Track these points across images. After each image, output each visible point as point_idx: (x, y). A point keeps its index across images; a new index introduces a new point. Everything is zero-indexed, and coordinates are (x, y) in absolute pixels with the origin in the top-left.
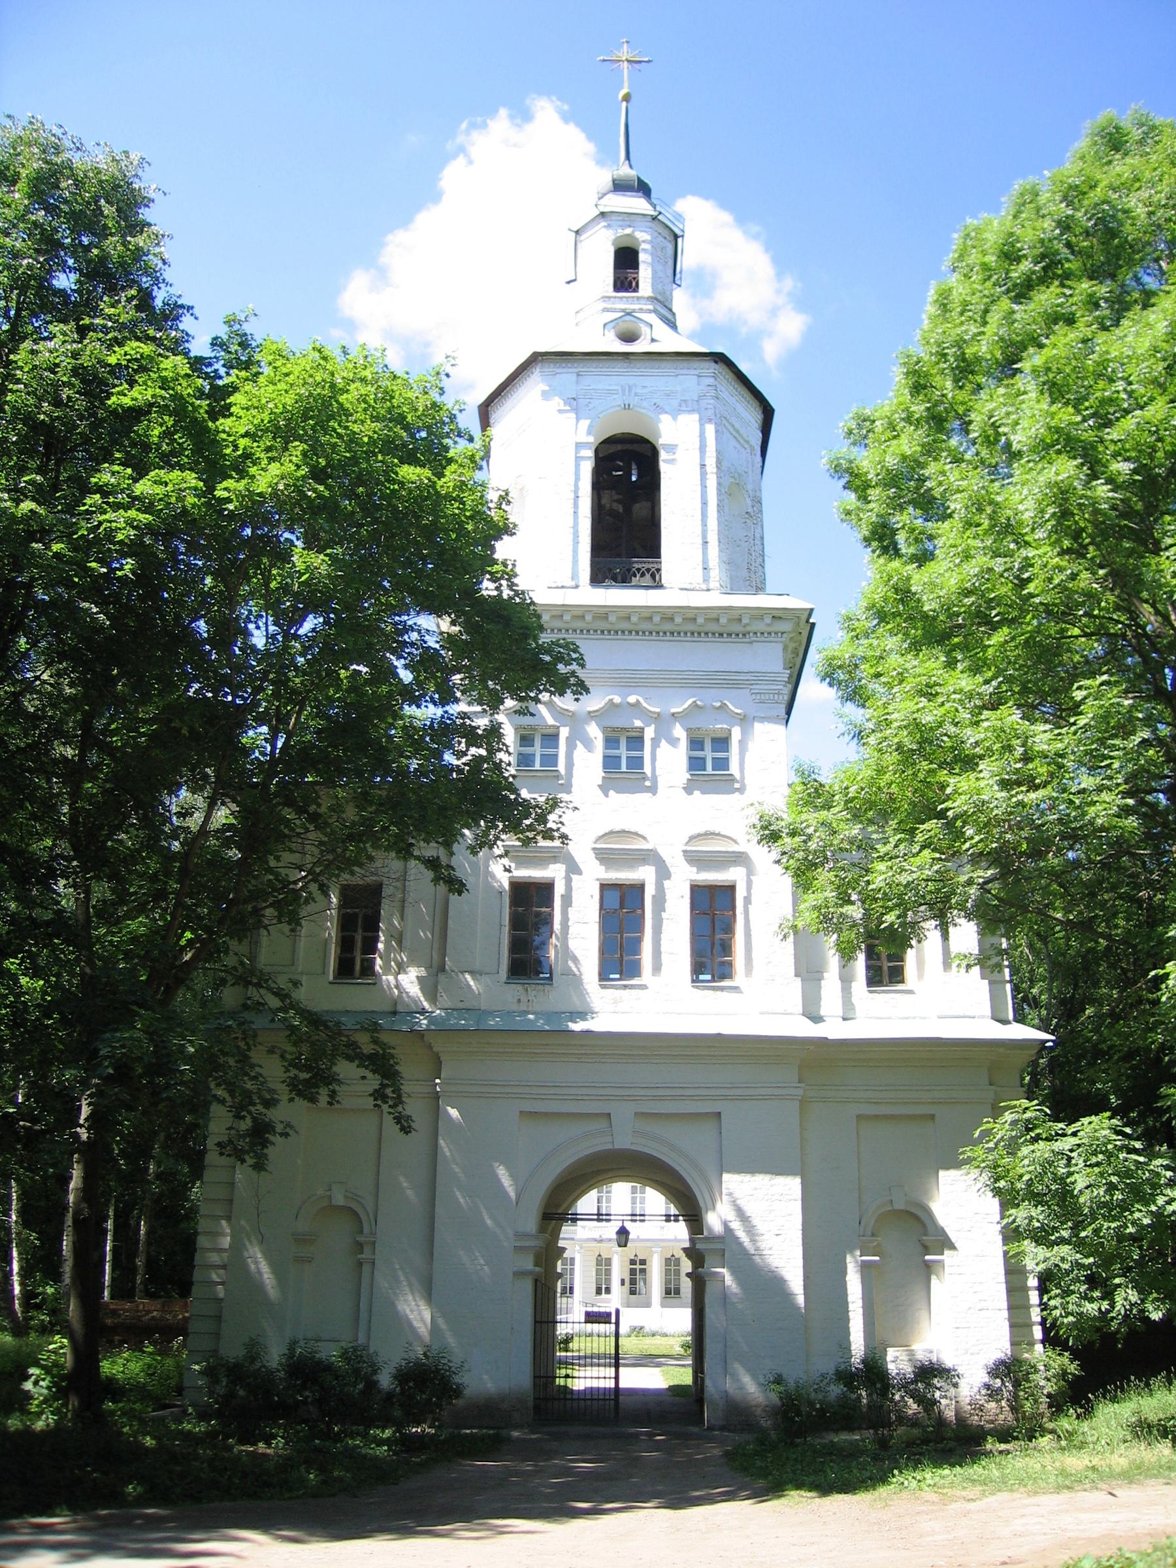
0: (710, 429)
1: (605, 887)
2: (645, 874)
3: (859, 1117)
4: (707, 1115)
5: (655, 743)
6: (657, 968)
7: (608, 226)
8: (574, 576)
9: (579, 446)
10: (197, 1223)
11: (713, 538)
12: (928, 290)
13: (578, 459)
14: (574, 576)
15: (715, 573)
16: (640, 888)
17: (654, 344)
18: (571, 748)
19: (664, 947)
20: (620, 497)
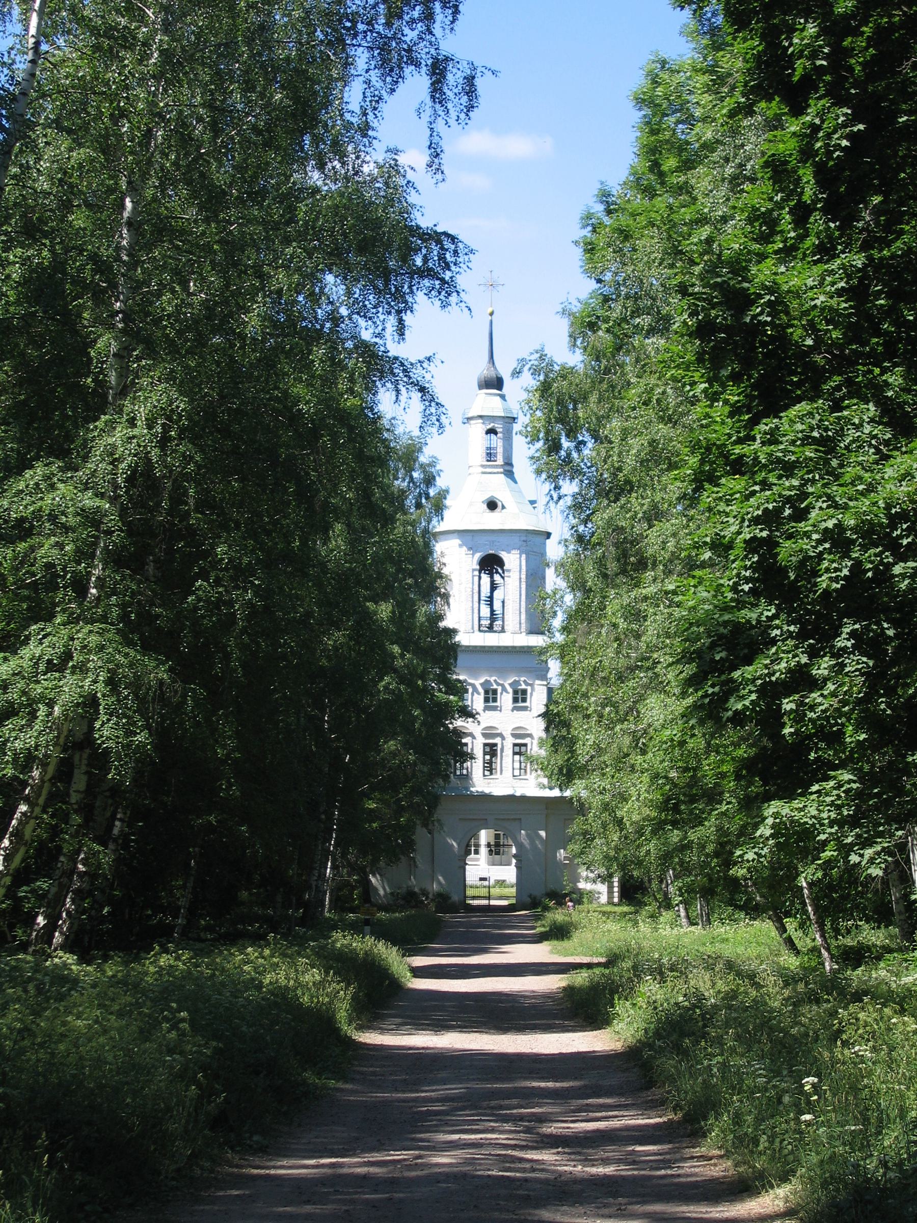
0: (524, 556)
1: (485, 745)
2: (498, 740)
3: (497, 819)
4: (515, 819)
5: (501, 694)
6: (501, 773)
7: (483, 423)
8: (473, 628)
9: (474, 570)
10: (414, 833)
11: (523, 610)
12: (396, 918)
13: (473, 576)
14: (473, 628)
15: (523, 626)
16: (496, 745)
17: (496, 514)
18: (473, 694)
19: (504, 765)
20: (459, 723)
